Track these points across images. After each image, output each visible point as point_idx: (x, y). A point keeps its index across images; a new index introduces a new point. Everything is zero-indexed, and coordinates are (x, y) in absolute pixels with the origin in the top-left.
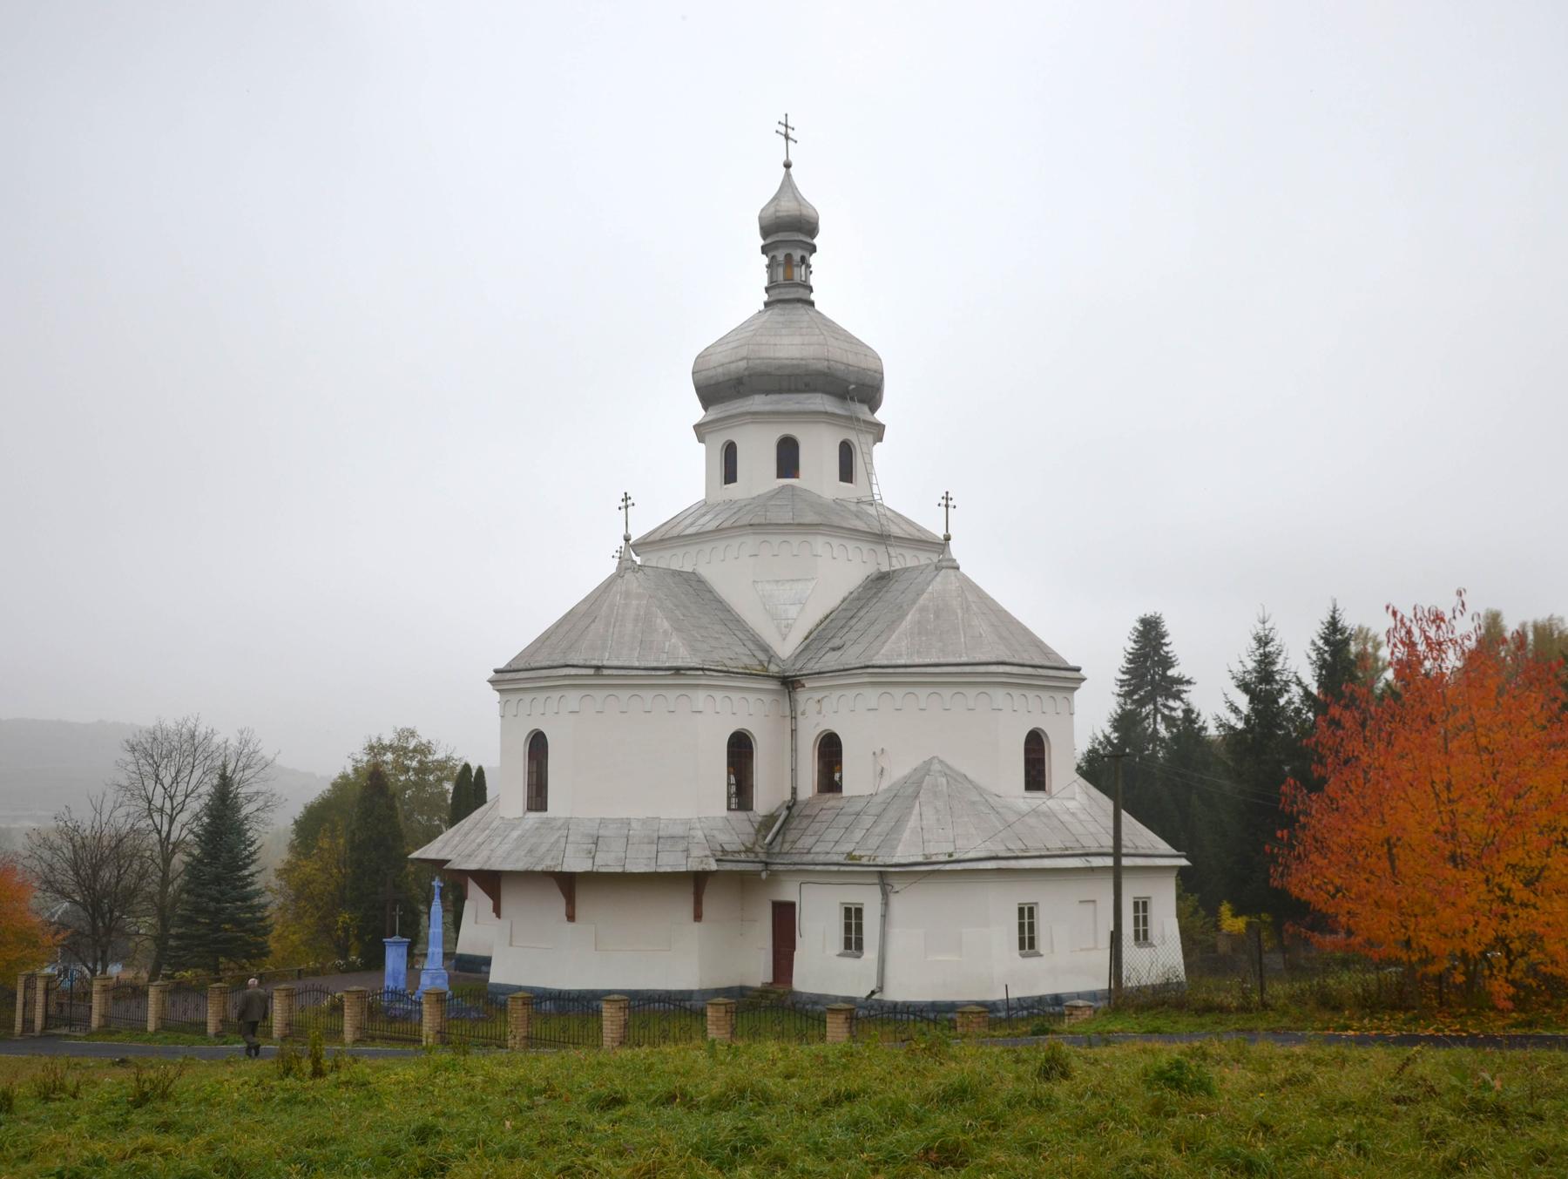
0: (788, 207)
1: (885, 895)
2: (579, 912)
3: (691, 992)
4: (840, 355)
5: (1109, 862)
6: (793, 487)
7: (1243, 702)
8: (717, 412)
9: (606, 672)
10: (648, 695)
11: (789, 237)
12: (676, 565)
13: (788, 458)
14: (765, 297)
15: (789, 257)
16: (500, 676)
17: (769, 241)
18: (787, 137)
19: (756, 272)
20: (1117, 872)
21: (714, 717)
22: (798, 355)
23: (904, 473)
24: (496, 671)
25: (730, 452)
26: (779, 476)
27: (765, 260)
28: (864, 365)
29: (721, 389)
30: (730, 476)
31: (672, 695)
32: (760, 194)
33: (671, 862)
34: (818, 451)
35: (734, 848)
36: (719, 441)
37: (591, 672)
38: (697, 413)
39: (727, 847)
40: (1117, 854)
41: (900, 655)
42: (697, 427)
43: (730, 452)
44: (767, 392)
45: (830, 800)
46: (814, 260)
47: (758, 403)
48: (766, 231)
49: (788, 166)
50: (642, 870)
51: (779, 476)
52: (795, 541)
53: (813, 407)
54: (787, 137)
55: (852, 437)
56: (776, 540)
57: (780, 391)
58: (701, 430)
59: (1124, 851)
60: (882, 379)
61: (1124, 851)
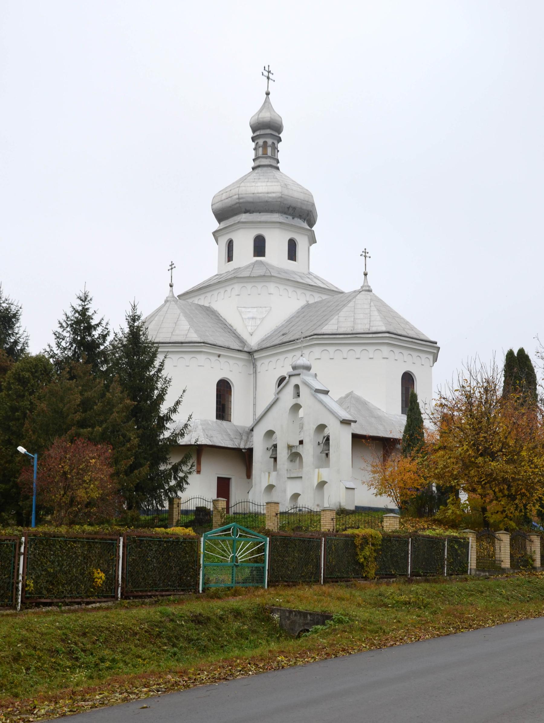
0: (266, 116)
4: (296, 194)
6: (261, 262)
8: (224, 224)
11: (267, 133)
12: (201, 303)
13: (259, 247)
14: (253, 164)
15: (265, 143)
17: (255, 134)
18: (268, 78)
19: (247, 150)
22: (302, 198)
25: (230, 245)
26: (254, 256)
27: (253, 145)
29: (227, 213)
30: (230, 258)
32: (251, 110)
36: (224, 241)
38: (215, 225)
42: (214, 233)
43: (230, 245)
45: (301, 446)
47: (244, 217)
48: (255, 128)
49: (268, 94)
51: (254, 256)
54: (268, 78)
58: (216, 234)
60: (313, 205)
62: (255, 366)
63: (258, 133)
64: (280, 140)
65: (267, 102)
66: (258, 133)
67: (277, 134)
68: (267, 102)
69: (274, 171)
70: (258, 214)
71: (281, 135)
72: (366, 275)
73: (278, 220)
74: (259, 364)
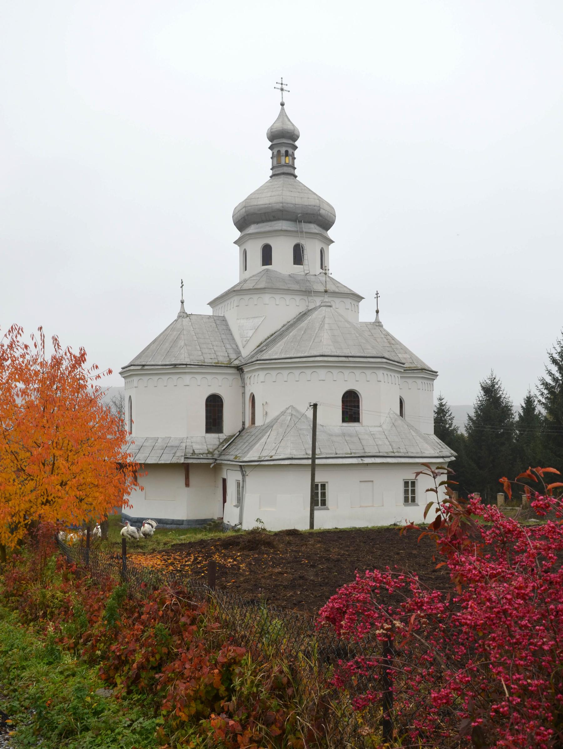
1: (243, 475)
2: (192, 480)
3: (183, 521)
5: (310, 462)
7: (554, 369)
9: (146, 367)
10: (165, 378)
11: (283, 141)
16: (124, 370)
18: (282, 90)
20: (313, 467)
21: (198, 389)
23: (346, 257)
24: (123, 368)
28: (306, 203)
29: (247, 219)
31: (175, 377)
32: (269, 120)
33: (167, 459)
34: (282, 251)
35: (201, 452)
37: (140, 367)
39: (196, 452)
40: (313, 458)
41: (277, 353)
44: (257, 223)
46: (297, 153)
49: (282, 104)
50: (152, 462)
51: (263, 265)
52: (255, 297)
53: (276, 228)
54: (282, 90)
55: (302, 242)
56: (246, 297)
57: (263, 221)
59: (317, 456)
61: (317, 456)
62: (243, 380)
63: (275, 142)
64: (295, 148)
65: (283, 112)
66: (275, 142)
67: (291, 142)
68: (283, 112)
69: (290, 179)
70: (256, 225)
71: (297, 143)
72: (182, 302)
73: (284, 228)
74: (247, 376)
